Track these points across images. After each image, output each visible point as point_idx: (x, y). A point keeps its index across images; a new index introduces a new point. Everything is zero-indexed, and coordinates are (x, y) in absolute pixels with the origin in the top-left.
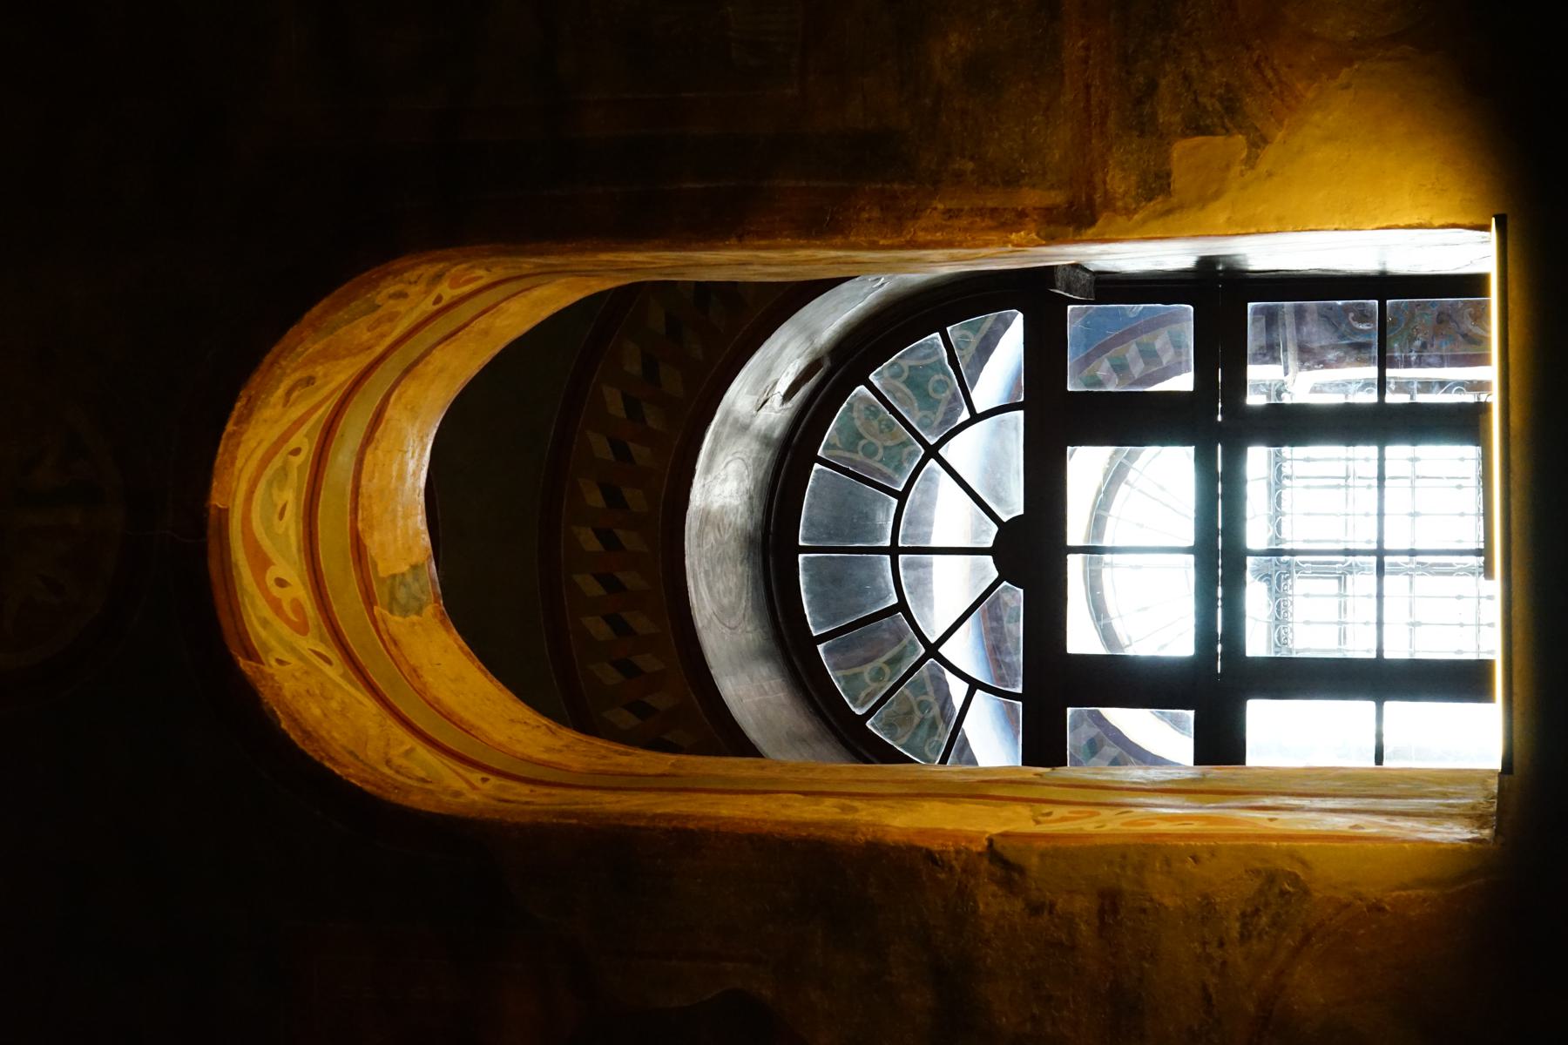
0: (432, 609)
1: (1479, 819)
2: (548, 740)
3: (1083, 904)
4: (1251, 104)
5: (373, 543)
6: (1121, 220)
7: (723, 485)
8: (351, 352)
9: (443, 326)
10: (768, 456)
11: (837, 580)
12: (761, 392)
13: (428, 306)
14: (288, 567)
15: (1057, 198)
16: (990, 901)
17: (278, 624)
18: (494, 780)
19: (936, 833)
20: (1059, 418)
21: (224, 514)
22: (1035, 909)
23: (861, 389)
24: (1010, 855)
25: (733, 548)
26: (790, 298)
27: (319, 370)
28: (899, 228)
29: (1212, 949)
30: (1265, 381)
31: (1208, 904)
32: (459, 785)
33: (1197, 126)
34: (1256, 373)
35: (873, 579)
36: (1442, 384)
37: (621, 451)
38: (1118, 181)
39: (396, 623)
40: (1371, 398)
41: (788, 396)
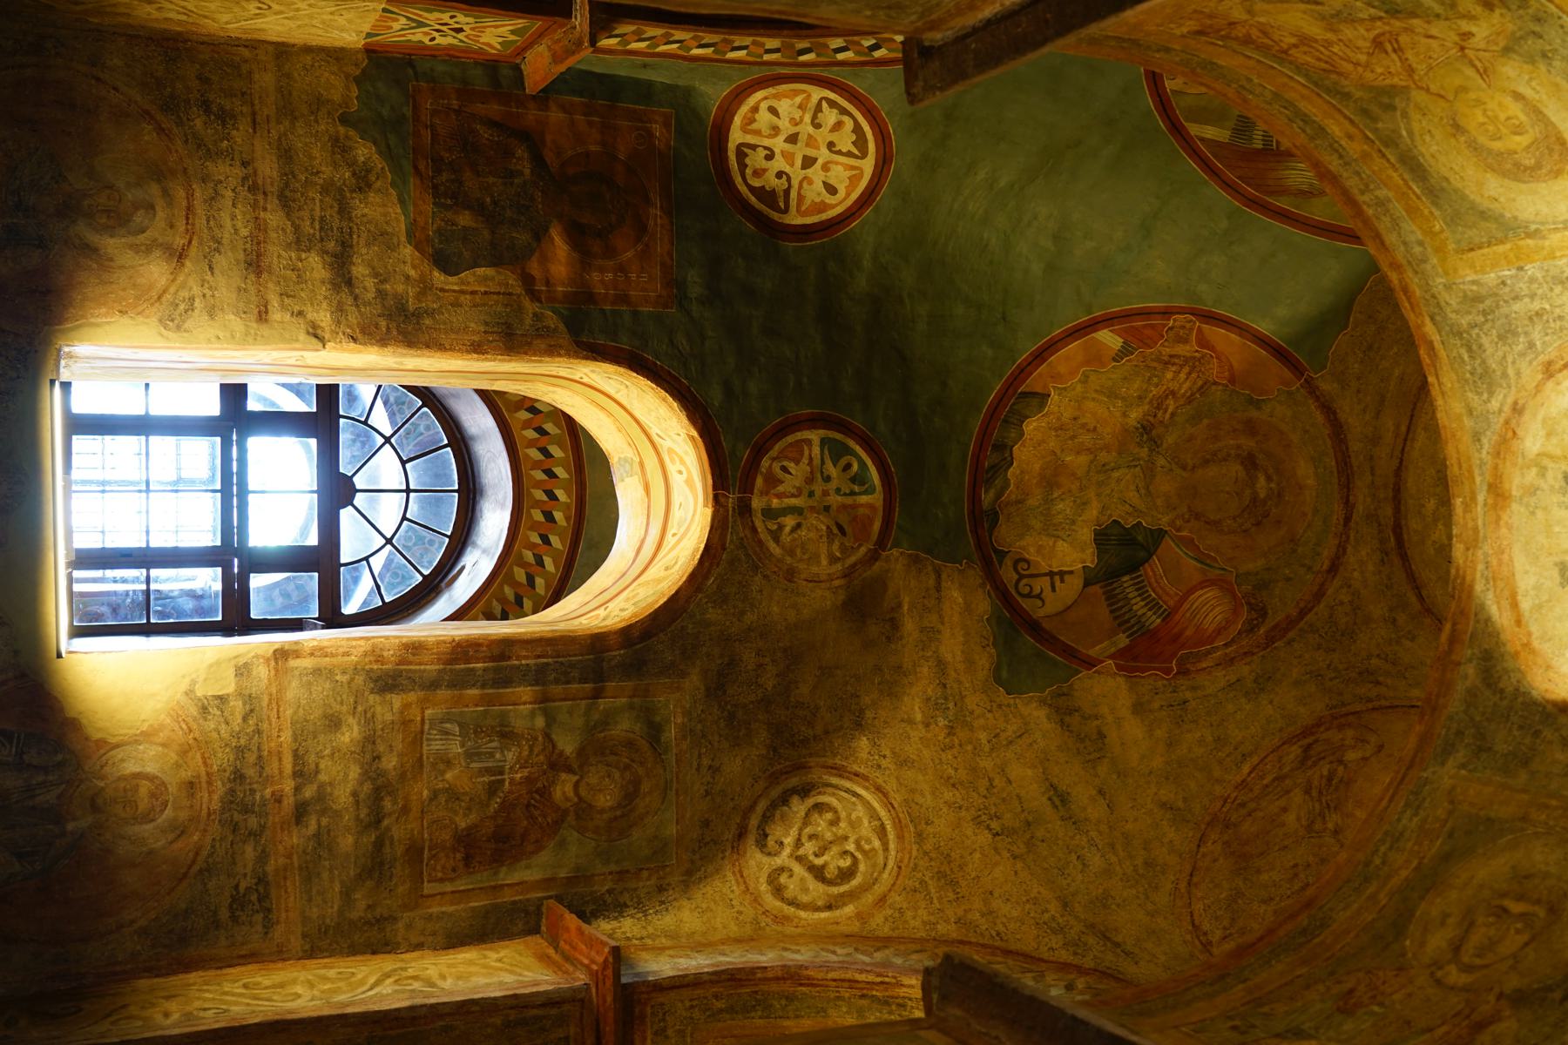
0: (614, 461)
1: (70, 356)
2: (556, 397)
3: (276, 315)
4: (194, 711)
5: (641, 492)
6: (260, 652)
7: (494, 522)
8: (647, 583)
9: (607, 596)
10: (474, 538)
11: (437, 476)
12: (477, 567)
13: (611, 605)
14: (677, 481)
15: (293, 663)
16: (324, 318)
17: (681, 453)
18: (577, 378)
19: (351, 351)
20: (321, 560)
21: (705, 505)
22: (300, 313)
23: (426, 572)
24: (314, 340)
25: (489, 492)
26: (458, 615)
27: (663, 573)
28: (374, 647)
29: (209, 293)
30: (209, 580)
31: (212, 316)
32: (593, 376)
33: (222, 699)
34: (218, 586)
35: (419, 477)
36: (115, 581)
37: (546, 540)
38: (262, 672)
39: (629, 453)
40: (154, 572)
41: (463, 568)
